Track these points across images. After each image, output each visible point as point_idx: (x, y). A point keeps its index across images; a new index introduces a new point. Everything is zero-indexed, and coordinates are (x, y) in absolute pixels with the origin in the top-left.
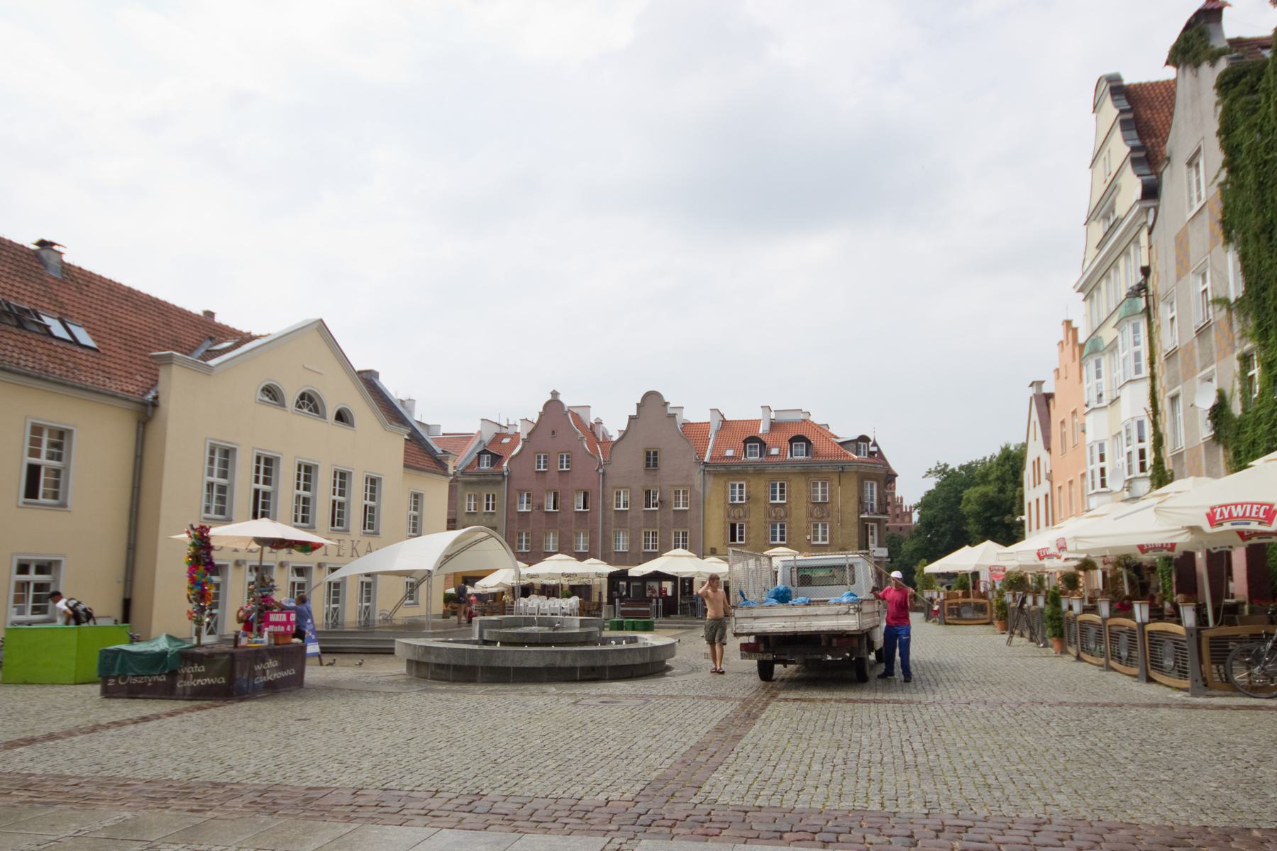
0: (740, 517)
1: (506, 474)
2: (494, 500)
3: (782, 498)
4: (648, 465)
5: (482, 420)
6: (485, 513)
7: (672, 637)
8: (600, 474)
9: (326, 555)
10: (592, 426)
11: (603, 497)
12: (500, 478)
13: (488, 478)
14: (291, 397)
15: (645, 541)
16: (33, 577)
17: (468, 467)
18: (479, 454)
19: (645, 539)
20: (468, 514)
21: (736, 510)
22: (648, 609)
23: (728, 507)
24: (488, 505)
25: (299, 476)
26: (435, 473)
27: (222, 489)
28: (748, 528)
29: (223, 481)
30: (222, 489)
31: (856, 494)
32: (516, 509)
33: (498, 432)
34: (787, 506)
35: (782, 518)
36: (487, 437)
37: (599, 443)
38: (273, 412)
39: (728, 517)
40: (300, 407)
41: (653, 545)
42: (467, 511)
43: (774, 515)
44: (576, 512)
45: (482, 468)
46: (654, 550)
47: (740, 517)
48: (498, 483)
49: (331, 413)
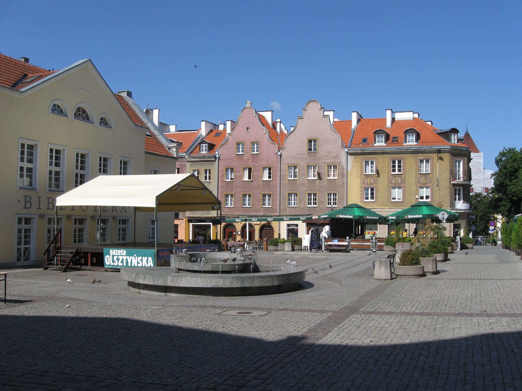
0: (371, 184)
2: (210, 173)
3: (399, 170)
4: (310, 149)
7: (215, 260)
16: (23, 226)
21: (369, 179)
23: (363, 176)
24: (206, 177)
25: (100, 164)
27: (30, 170)
28: (377, 191)
29: (30, 165)
30: (30, 170)
31: (449, 168)
34: (403, 176)
35: (399, 184)
38: (58, 118)
39: (364, 183)
40: (77, 116)
41: (314, 203)
43: (394, 182)
46: (315, 206)
47: (371, 184)
49: (96, 120)
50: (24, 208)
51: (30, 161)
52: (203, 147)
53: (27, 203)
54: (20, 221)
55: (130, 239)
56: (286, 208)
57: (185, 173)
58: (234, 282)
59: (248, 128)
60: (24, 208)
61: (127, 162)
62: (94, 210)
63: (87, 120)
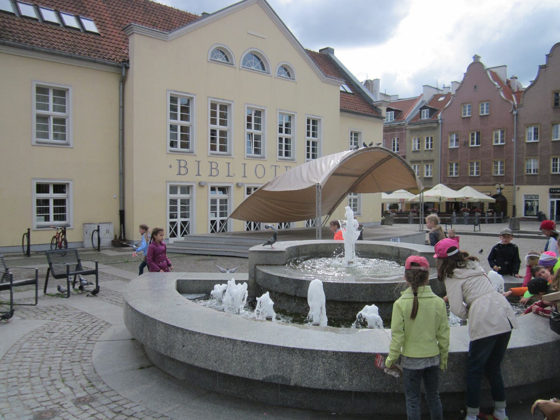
1: (440, 122)
2: (431, 141)
5: (423, 86)
6: (426, 151)
8: (514, 115)
9: (245, 176)
10: (508, 82)
11: (517, 133)
12: (435, 125)
13: (427, 126)
14: (238, 56)
15: (553, 166)
16: (179, 196)
17: (413, 120)
18: (421, 109)
19: (554, 164)
20: (414, 152)
26: (369, 116)
32: (447, 146)
36: (427, 98)
37: (514, 93)
42: (413, 150)
44: (494, 146)
45: (422, 119)
48: (435, 129)
50: (177, 175)
52: (424, 113)
53: (181, 168)
54: (173, 190)
55: (432, 204)
56: (523, 176)
58: (344, 372)
59: (475, 87)
60: (177, 175)
61: (317, 121)
63: (263, 70)
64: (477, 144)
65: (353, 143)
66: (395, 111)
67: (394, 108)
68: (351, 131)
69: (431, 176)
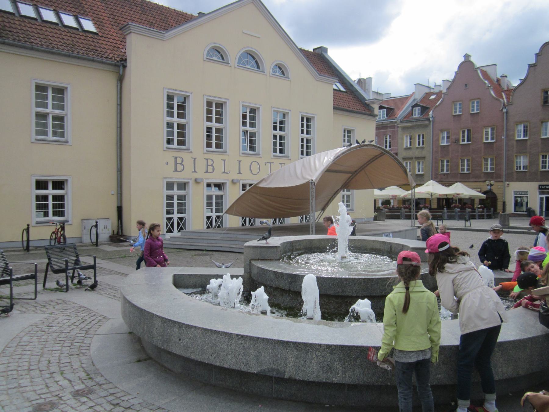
1: (431, 119)
2: (423, 138)
5: (415, 84)
6: (417, 148)
8: (503, 113)
10: (498, 80)
11: (507, 131)
12: (427, 122)
13: (418, 123)
14: (233, 55)
15: (543, 163)
16: (176, 192)
17: (405, 117)
18: (413, 107)
19: (543, 161)
20: (406, 149)
22: (399, 214)
26: (362, 113)
32: (439, 143)
33: (428, 92)
36: (419, 96)
37: (504, 91)
42: (405, 147)
44: (485, 143)
45: (414, 116)
48: (426, 126)
50: (174, 171)
51: (219, 121)
52: (415, 111)
53: (178, 165)
54: (170, 186)
55: (424, 200)
56: (513, 173)
57: (334, 113)
59: (466, 85)
60: (174, 171)
61: (311, 119)
62: (174, 170)
64: (468, 141)
65: (346, 141)
66: (387, 109)
67: (387, 106)
68: (344, 128)
69: (423, 173)
